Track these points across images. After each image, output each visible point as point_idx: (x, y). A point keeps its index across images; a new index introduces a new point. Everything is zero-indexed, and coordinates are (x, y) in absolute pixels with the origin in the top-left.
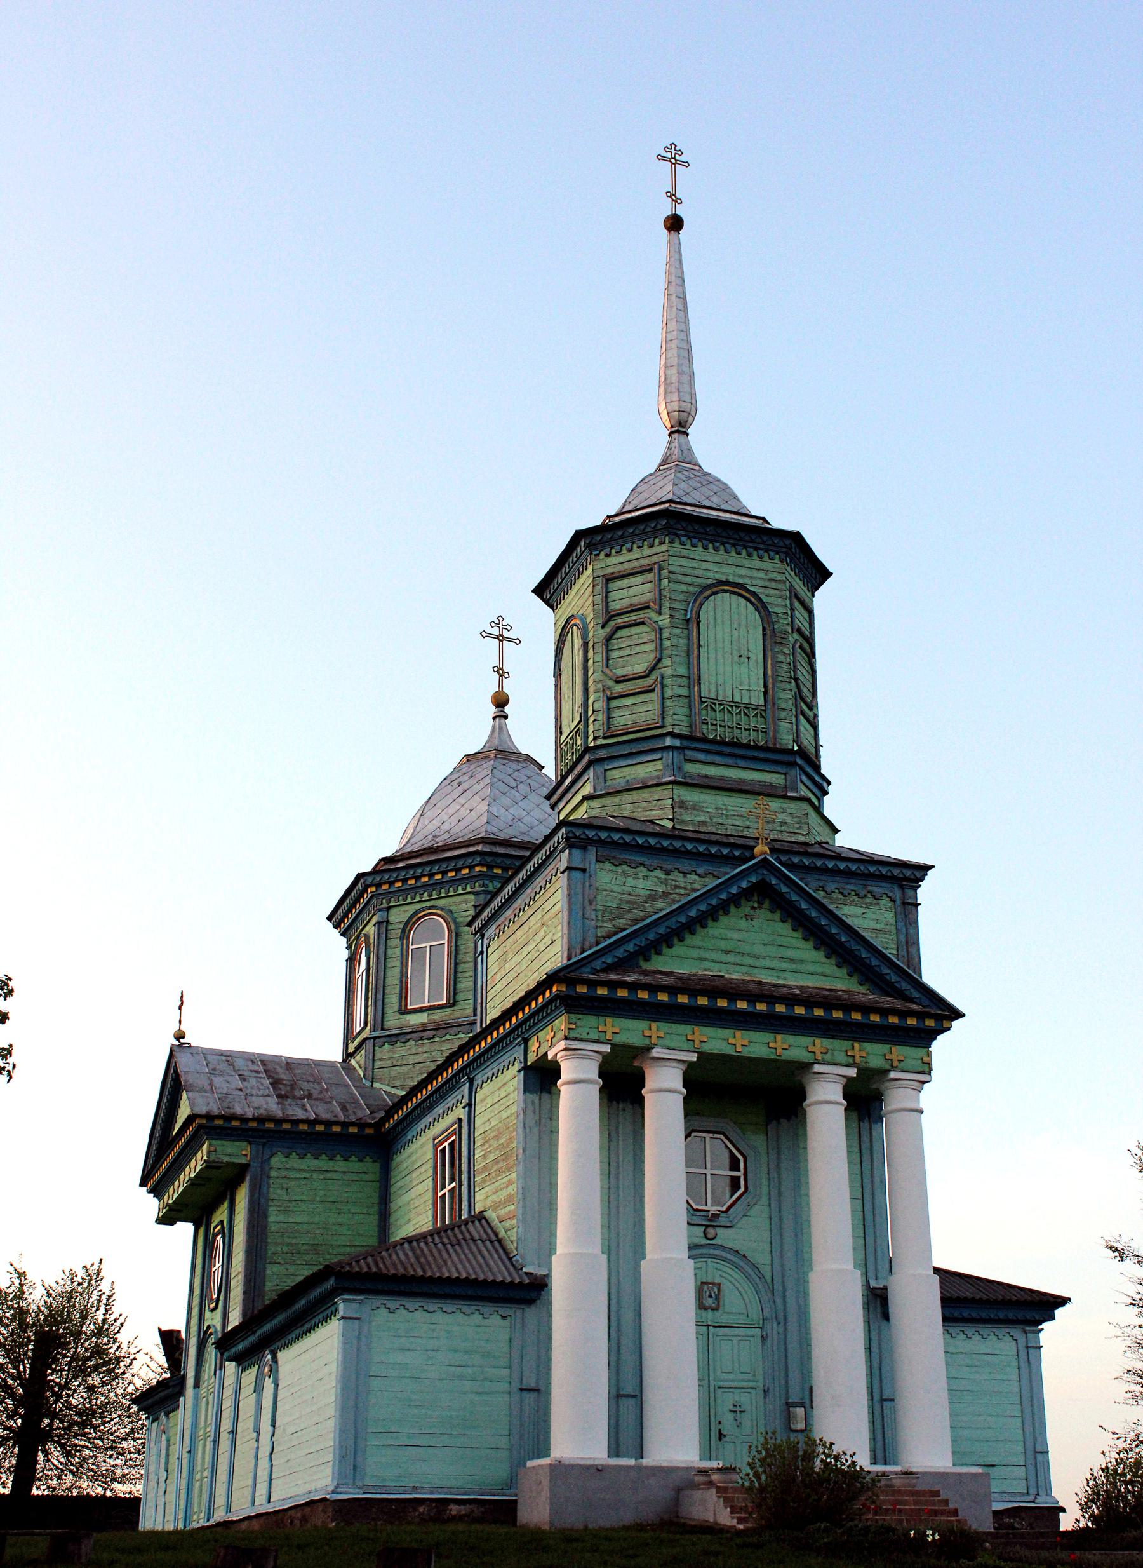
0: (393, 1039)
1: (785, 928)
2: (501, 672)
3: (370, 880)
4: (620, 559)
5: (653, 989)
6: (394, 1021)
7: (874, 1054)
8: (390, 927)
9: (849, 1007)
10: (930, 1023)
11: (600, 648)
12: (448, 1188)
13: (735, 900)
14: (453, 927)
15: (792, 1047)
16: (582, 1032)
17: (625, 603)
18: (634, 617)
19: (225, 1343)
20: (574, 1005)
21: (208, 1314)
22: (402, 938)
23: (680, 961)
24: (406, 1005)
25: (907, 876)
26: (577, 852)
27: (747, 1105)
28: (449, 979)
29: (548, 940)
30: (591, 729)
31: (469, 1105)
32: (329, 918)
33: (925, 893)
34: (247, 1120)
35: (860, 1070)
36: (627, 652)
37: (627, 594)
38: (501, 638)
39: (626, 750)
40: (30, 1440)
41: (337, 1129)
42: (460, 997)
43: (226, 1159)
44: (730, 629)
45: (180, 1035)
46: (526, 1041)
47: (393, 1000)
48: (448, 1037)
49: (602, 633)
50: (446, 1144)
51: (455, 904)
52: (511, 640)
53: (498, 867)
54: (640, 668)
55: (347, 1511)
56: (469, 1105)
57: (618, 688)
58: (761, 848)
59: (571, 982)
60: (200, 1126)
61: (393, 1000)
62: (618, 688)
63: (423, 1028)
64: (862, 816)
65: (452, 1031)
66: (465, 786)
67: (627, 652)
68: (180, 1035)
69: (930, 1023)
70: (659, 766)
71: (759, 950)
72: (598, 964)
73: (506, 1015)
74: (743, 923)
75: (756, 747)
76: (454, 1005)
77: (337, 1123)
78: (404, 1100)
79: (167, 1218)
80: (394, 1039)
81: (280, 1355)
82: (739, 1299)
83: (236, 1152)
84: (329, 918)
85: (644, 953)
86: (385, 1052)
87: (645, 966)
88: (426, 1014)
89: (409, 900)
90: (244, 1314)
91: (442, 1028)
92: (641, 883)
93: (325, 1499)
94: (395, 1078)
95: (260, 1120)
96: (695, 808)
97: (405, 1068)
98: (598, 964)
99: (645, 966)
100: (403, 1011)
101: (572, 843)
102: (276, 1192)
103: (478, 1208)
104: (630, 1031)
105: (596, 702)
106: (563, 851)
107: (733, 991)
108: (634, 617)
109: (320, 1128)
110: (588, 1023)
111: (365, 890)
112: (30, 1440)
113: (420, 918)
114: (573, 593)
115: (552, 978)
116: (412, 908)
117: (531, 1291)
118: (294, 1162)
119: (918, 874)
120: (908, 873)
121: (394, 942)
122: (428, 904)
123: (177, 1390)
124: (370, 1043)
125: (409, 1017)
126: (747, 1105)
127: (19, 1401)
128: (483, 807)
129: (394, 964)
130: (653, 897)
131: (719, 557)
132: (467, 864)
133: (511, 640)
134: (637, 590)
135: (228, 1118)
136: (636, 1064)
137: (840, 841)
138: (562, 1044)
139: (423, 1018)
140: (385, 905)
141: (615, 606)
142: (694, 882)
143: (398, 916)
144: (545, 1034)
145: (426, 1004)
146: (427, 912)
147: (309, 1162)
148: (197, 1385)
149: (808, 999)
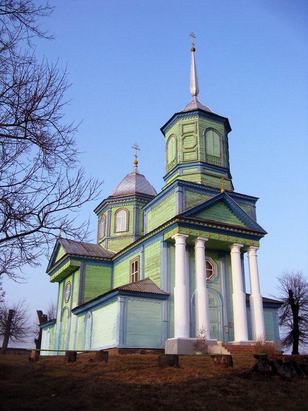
0: (113, 238)
1: (206, 211)
2: (136, 156)
3: (107, 201)
4: (189, 120)
5: (199, 222)
6: (112, 234)
7: (248, 242)
9: (242, 229)
10: (260, 235)
11: (181, 141)
12: (135, 273)
13: (216, 202)
15: (232, 239)
16: (182, 232)
17: (188, 131)
18: (190, 134)
19: (73, 311)
20: (180, 225)
21: (64, 304)
23: (205, 216)
25: (253, 200)
26: (181, 188)
27: (218, 252)
29: (170, 210)
30: (178, 160)
31: (143, 252)
33: (257, 204)
34: (80, 255)
35: (244, 245)
36: (188, 142)
37: (186, 129)
38: (136, 148)
39: (188, 165)
40: (7, 335)
41: (102, 259)
43: (75, 265)
44: (214, 141)
46: (163, 235)
47: (112, 230)
49: (181, 138)
54: (191, 146)
55: (122, 351)
56: (143, 252)
57: (186, 151)
58: (222, 191)
59: (180, 219)
60: (69, 256)
61: (112, 230)
62: (186, 151)
63: (120, 237)
64: (241, 187)
67: (188, 142)
69: (260, 235)
70: (196, 169)
71: (221, 215)
72: (187, 215)
73: (151, 232)
74: (218, 208)
75: (218, 167)
77: (101, 257)
78: (116, 255)
79: (53, 281)
81: (93, 313)
82: (217, 302)
83: (78, 263)
84: (163, 178)
85: (196, 213)
86: (110, 242)
87: (196, 216)
90: (79, 303)
91: (125, 236)
92: (195, 196)
95: (83, 256)
98: (187, 215)
99: (196, 216)
101: (179, 185)
102: (87, 274)
103: (146, 277)
104: (194, 232)
105: (180, 154)
106: (176, 187)
107: (213, 223)
108: (190, 134)
109: (98, 258)
110: (186, 230)
112: (7, 335)
114: (172, 128)
115: (176, 217)
117: (165, 297)
118: (91, 266)
119: (256, 200)
120: (253, 199)
121: (113, 216)
124: (106, 240)
126: (218, 252)
127: (5, 326)
128: (134, 186)
129: (113, 221)
130: (197, 200)
131: (209, 122)
134: (191, 128)
135: (75, 255)
136: (193, 241)
137: (234, 191)
138: (178, 234)
139: (120, 234)
141: (185, 131)
142: (207, 197)
143: (114, 210)
144: (172, 232)
148: (61, 321)
149: (234, 227)
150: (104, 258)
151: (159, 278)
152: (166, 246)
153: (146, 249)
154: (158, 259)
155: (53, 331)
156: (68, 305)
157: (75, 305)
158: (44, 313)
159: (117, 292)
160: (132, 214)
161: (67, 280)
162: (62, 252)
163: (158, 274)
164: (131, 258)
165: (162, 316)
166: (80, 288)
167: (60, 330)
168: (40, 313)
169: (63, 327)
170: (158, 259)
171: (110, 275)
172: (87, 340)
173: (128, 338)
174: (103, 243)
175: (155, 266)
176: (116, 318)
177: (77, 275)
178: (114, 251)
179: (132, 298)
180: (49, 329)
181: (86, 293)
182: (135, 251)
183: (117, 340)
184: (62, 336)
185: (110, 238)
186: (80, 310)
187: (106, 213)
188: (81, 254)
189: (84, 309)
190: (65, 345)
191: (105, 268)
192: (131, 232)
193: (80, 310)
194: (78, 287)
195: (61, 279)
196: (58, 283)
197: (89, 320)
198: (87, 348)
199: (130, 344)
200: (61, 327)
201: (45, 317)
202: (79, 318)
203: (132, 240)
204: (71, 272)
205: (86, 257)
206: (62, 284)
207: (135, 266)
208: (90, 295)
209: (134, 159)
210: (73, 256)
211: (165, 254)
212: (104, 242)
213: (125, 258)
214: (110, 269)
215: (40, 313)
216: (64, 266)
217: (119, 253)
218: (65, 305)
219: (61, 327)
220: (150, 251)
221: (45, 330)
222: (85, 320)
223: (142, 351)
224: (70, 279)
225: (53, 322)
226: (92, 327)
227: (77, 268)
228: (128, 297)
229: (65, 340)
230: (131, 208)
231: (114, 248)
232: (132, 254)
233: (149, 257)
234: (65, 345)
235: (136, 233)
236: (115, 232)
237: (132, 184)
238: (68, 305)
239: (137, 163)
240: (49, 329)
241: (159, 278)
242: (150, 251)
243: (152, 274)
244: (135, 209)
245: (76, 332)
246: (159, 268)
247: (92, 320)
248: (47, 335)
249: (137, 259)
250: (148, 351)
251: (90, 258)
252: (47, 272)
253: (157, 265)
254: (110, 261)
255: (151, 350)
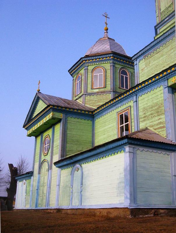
0: (90, 94)
2: (106, 23)
3: (84, 59)
6: (89, 91)
8: (88, 70)
14: (105, 70)
19: (56, 163)
22: (92, 73)
24: (93, 87)
28: (104, 83)
32: (69, 71)
34: (62, 107)
38: (106, 17)
41: (83, 112)
42: (107, 86)
43: (57, 117)
45: (39, 91)
46: (168, 79)
47: (89, 86)
48: (104, 94)
50: (123, 113)
51: (105, 65)
52: (108, 18)
53: (116, 58)
55: (135, 212)
61: (89, 86)
63: (98, 93)
65: (105, 93)
66: (103, 43)
68: (39, 91)
73: (144, 82)
76: (106, 87)
78: (96, 110)
79: (30, 135)
80: (90, 95)
81: (83, 165)
86: (88, 98)
88: (98, 90)
89: (93, 64)
90: (62, 156)
93: (127, 208)
94: (91, 104)
96: (168, 108)
97: (94, 101)
100: (92, 89)
102: (69, 126)
109: (79, 111)
111: (82, 62)
113: (96, 68)
116: (94, 66)
118: (73, 119)
122: (98, 65)
123: (31, 175)
125: (94, 90)
128: (109, 47)
132: (109, 56)
133: (108, 18)
135: (58, 106)
140: (87, 65)
143: (90, 68)
145: (98, 87)
146: (98, 67)
147: (76, 120)
148: (39, 173)
150: (85, 111)
151: (163, 127)
152: (171, 92)
153: (140, 98)
154: (160, 107)
155: (30, 182)
156: (48, 158)
157: (56, 158)
158: (15, 165)
159: (126, 141)
160: (109, 72)
161: (45, 134)
162: (41, 106)
163: (160, 123)
164: (120, 109)
165: (172, 170)
166: (62, 140)
167: (39, 182)
168: (11, 166)
169: (42, 179)
170: (160, 107)
171: (90, 128)
172: (75, 195)
173: (139, 196)
174: (79, 99)
175: (156, 115)
176: (122, 170)
177: (58, 128)
178: (92, 106)
179: (141, 149)
180: (24, 181)
181: (68, 145)
182: (124, 102)
183: (126, 198)
184: (41, 188)
185: (87, 94)
186: (65, 163)
187: (82, 71)
188: (63, 106)
189: (72, 161)
190: (45, 197)
191: (86, 121)
192: (109, 87)
193: (65, 163)
194: (61, 139)
195: (37, 134)
196: (34, 137)
197: (78, 174)
198: (75, 204)
199: (142, 204)
200: (39, 179)
201: (16, 169)
202: (62, 171)
203: (110, 96)
204: (51, 125)
205: (68, 109)
206: (39, 139)
207: (124, 119)
208: (73, 149)
209: (104, 27)
210: (55, 107)
211: (171, 100)
212: (82, 98)
213: (110, 110)
214: (91, 122)
215: (11, 166)
216: (34, 127)
217: (98, 108)
218: (43, 157)
219: (39, 179)
220: (146, 99)
221: (20, 181)
222: (72, 174)
223: (155, 212)
224: (50, 132)
225: (30, 174)
226: (82, 182)
227: (59, 121)
228: (137, 147)
229: (45, 192)
230: (108, 66)
231: (92, 103)
232: (119, 105)
233: (145, 106)
234: (45, 197)
235: (113, 89)
236: (92, 89)
237: (106, 46)
238: (48, 158)
239: (107, 30)
240: (24, 181)
241: (163, 127)
242: (146, 99)
243: (151, 124)
244: (112, 67)
245: (59, 185)
246: (163, 117)
247: (82, 173)
248: (22, 186)
249: (128, 109)
250: (162, 211)
251: (72, 110)
252: (24, 127)
253: (159, 113)
254: (91, 115)
255: (165, 210)
